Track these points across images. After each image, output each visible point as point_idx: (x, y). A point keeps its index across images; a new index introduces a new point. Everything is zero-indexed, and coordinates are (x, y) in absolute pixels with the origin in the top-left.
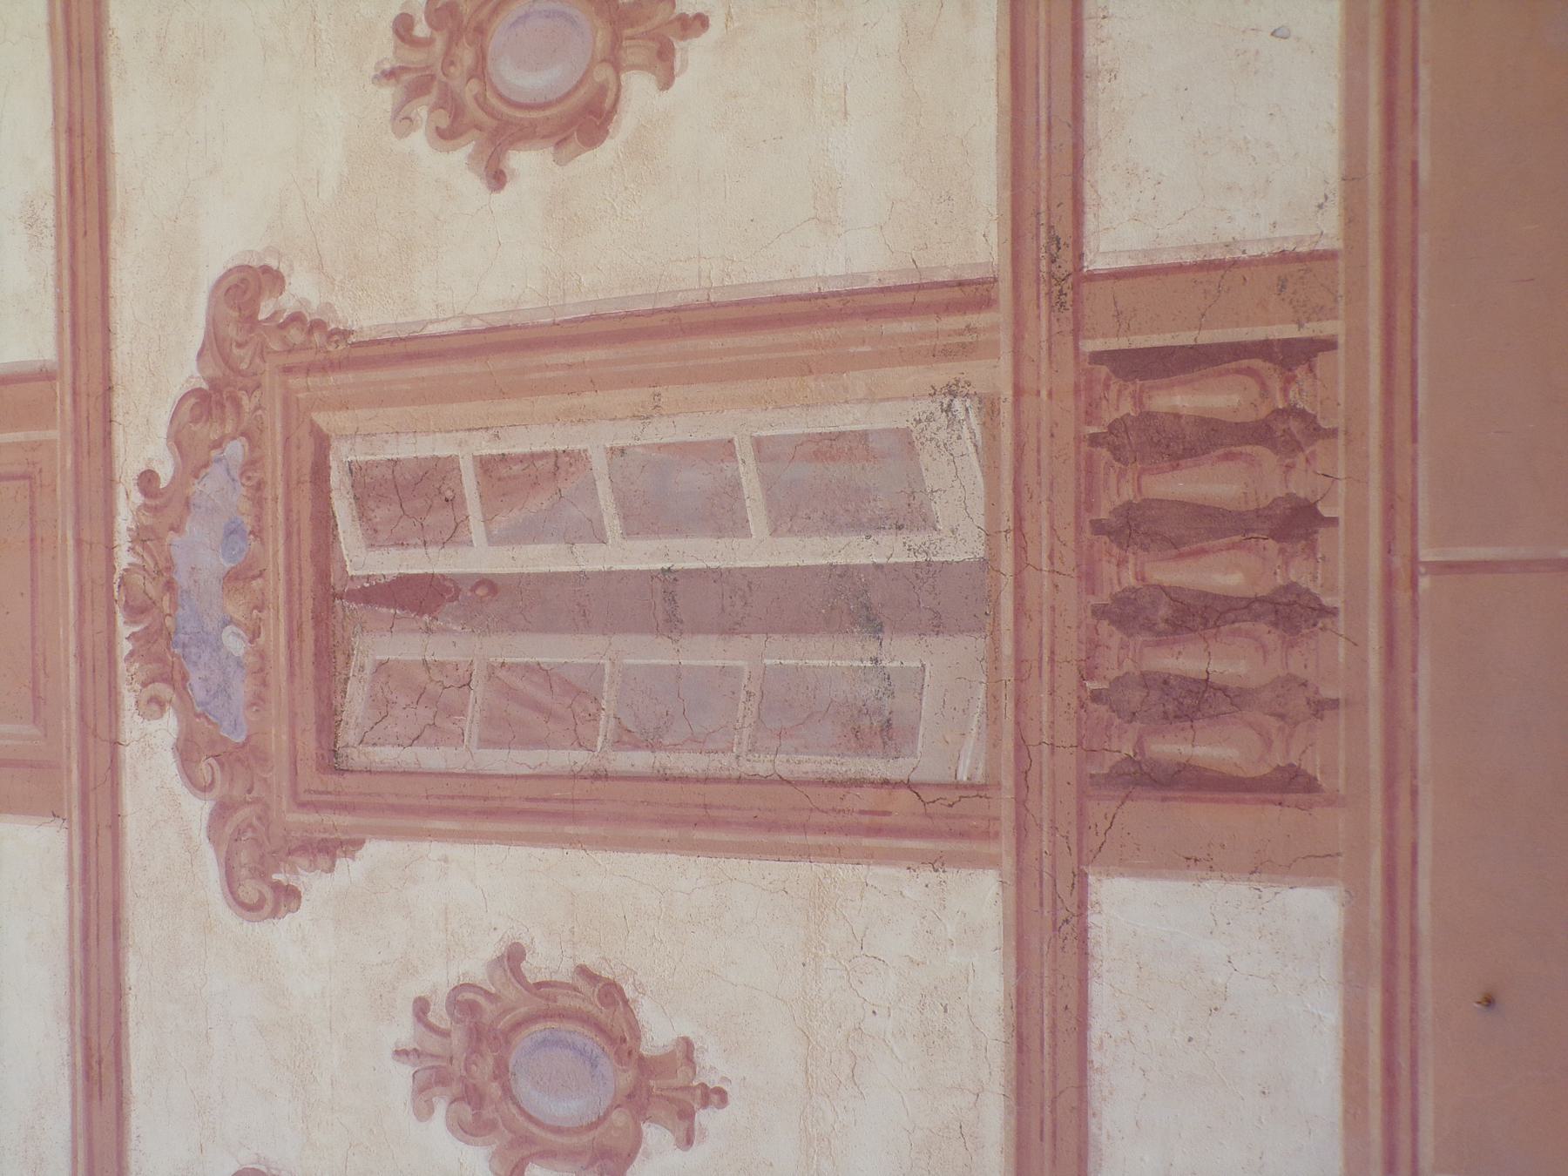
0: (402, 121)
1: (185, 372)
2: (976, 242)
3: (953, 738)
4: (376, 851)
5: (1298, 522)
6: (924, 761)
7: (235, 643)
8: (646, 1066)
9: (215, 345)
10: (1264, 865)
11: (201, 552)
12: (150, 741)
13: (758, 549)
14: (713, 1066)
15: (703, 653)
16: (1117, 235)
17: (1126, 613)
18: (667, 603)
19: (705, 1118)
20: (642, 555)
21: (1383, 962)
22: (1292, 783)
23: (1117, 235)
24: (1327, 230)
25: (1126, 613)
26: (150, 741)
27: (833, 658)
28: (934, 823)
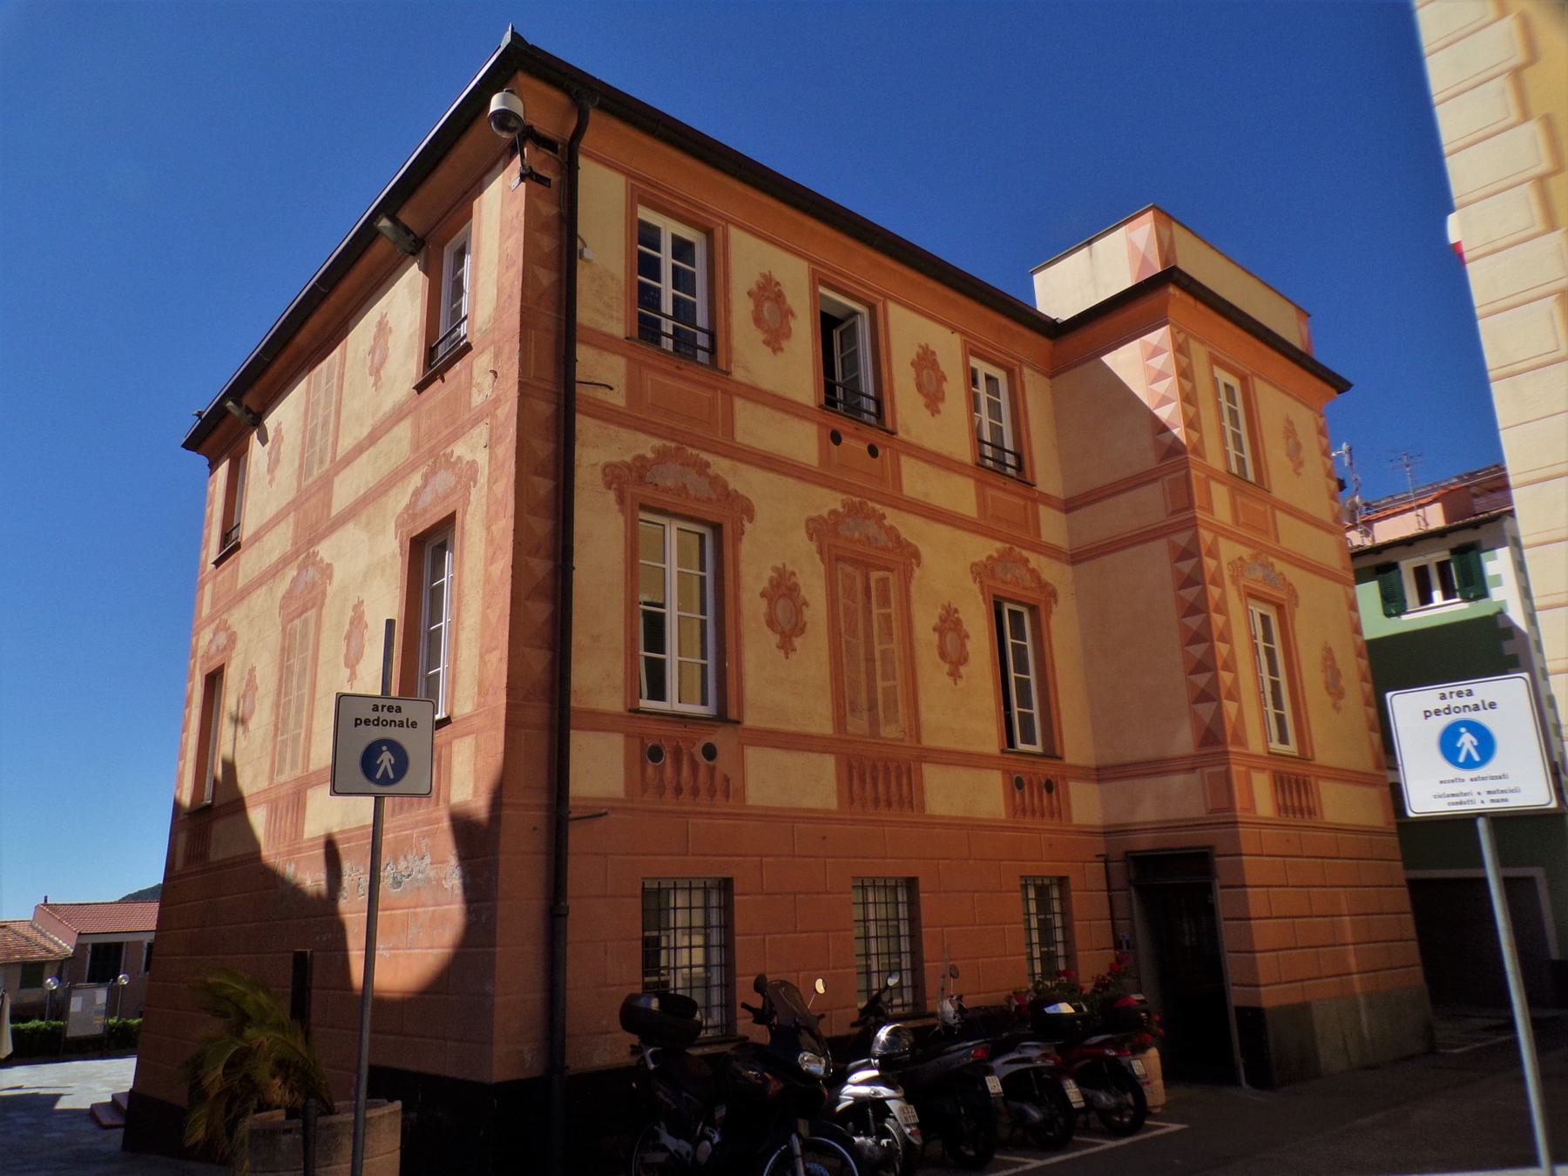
0: (943, 607)
1: (734, 485)
2: (928, 741)
3: (858, 725)
4: (822, 567)
5: (889, 804)
6: (849, 718)
7: (857, 535)
8: (790, 638)
9: (909, 545)
10: (840, 793)
11: (872, 529)
12: (647, 445)
13: (880, 684)
14: (793, 656)
15: (863, 665)
16: (928, 769)
17: (874, 767)
18: (870, 659)
19: (782, 653)
20: (877, 655)
21: (992, 827)
22: (852, 801)
23: (928, 769)
24: (750, 802)
25: (874, 767)
26: (647, 445)
27: (863, 700)
28: (840, 721)
